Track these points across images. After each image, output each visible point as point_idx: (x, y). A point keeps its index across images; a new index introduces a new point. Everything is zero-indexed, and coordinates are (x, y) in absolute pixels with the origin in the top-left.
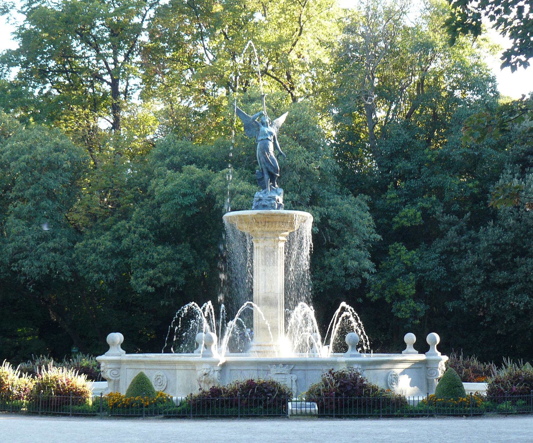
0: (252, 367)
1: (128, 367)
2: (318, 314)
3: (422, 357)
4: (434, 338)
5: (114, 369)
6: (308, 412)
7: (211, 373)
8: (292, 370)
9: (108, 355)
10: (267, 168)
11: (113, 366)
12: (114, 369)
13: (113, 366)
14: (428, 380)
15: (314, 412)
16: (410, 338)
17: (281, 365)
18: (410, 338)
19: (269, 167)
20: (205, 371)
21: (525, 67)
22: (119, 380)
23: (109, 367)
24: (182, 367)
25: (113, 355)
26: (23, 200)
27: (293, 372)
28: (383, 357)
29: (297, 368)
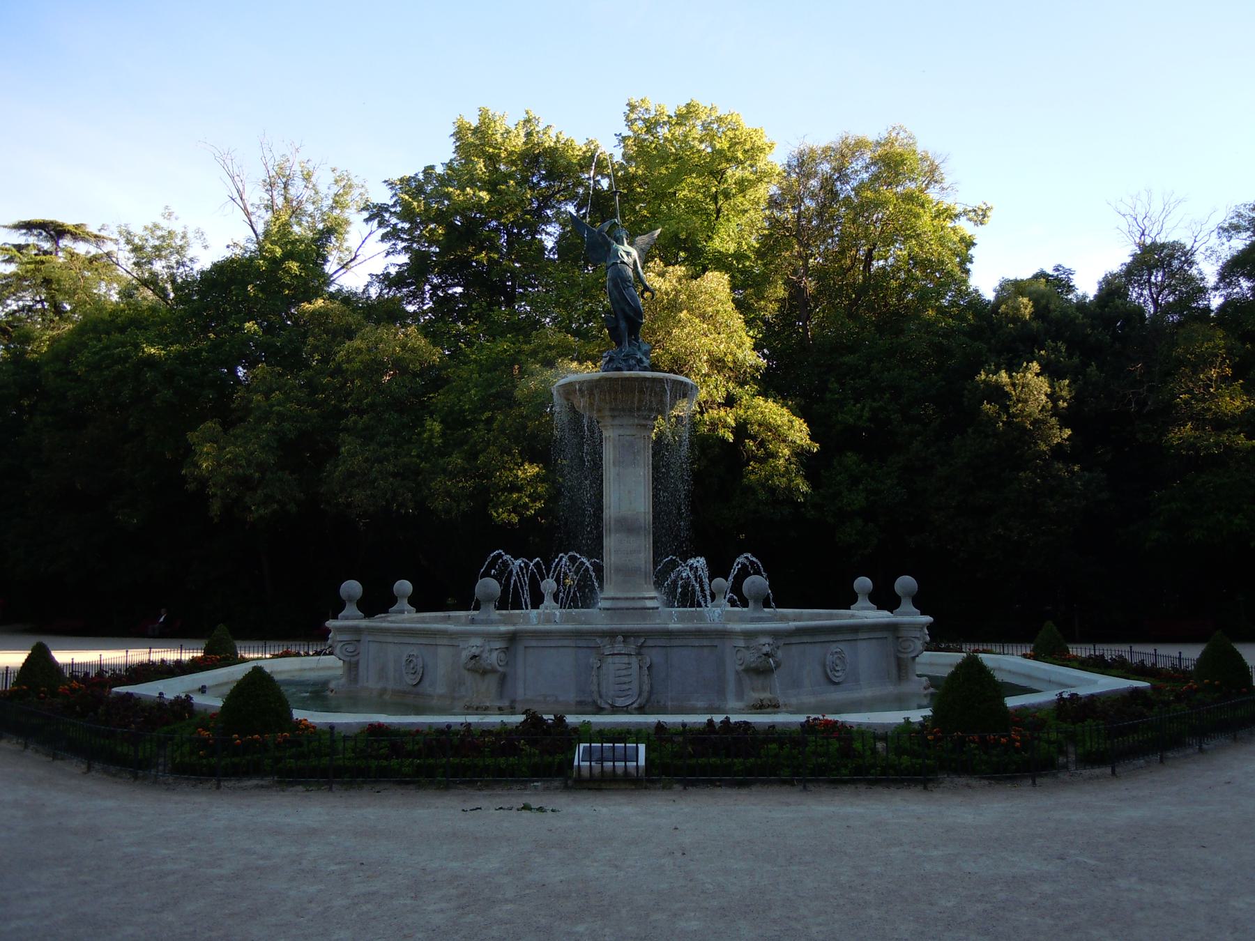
0: (566, 643)
1: (370, 638)
2: (233, 270)
3: (883, 616)
4: (905, 583)
5: (349, 643)
6: (620, 771)
7: (484, 655)
8: (641, 647)
9: (897, 615)
10: (623, 310)
11: (346, 637)
12: (349, 643)
13: (346, 637)
14: (898, 659)
15: (633, 771)
16: (863, 583)
17: (620, 638)
18: (863, 583)
19: (627, 309)
20: (475, 651)
21: (974, 244)
22: (357, 663)
23: (338, 638)
24: (445, 642)
25: (347, 618)
26: (360, 412)
27: (644, 651)
28: (819, 617)
29: (650, 643)
